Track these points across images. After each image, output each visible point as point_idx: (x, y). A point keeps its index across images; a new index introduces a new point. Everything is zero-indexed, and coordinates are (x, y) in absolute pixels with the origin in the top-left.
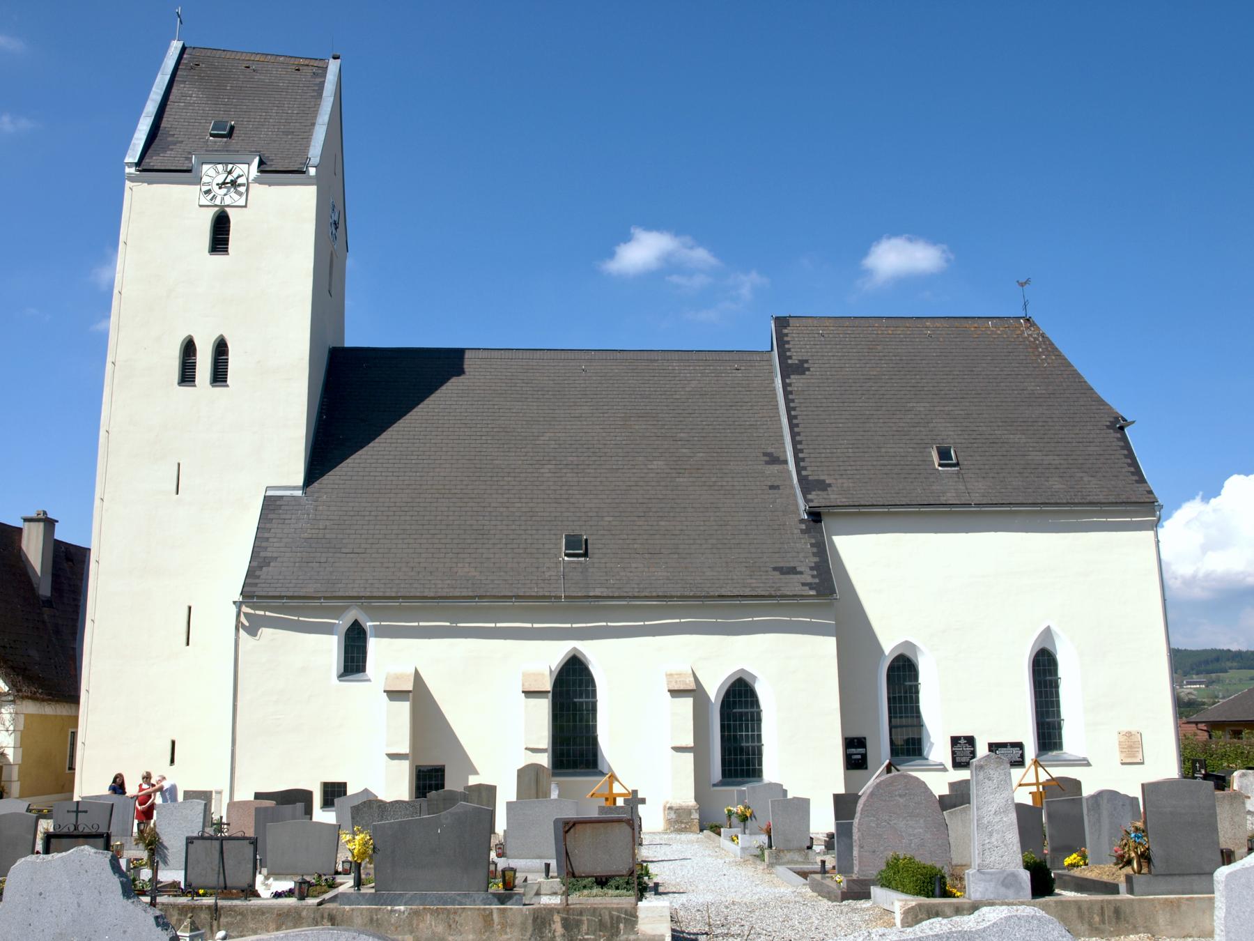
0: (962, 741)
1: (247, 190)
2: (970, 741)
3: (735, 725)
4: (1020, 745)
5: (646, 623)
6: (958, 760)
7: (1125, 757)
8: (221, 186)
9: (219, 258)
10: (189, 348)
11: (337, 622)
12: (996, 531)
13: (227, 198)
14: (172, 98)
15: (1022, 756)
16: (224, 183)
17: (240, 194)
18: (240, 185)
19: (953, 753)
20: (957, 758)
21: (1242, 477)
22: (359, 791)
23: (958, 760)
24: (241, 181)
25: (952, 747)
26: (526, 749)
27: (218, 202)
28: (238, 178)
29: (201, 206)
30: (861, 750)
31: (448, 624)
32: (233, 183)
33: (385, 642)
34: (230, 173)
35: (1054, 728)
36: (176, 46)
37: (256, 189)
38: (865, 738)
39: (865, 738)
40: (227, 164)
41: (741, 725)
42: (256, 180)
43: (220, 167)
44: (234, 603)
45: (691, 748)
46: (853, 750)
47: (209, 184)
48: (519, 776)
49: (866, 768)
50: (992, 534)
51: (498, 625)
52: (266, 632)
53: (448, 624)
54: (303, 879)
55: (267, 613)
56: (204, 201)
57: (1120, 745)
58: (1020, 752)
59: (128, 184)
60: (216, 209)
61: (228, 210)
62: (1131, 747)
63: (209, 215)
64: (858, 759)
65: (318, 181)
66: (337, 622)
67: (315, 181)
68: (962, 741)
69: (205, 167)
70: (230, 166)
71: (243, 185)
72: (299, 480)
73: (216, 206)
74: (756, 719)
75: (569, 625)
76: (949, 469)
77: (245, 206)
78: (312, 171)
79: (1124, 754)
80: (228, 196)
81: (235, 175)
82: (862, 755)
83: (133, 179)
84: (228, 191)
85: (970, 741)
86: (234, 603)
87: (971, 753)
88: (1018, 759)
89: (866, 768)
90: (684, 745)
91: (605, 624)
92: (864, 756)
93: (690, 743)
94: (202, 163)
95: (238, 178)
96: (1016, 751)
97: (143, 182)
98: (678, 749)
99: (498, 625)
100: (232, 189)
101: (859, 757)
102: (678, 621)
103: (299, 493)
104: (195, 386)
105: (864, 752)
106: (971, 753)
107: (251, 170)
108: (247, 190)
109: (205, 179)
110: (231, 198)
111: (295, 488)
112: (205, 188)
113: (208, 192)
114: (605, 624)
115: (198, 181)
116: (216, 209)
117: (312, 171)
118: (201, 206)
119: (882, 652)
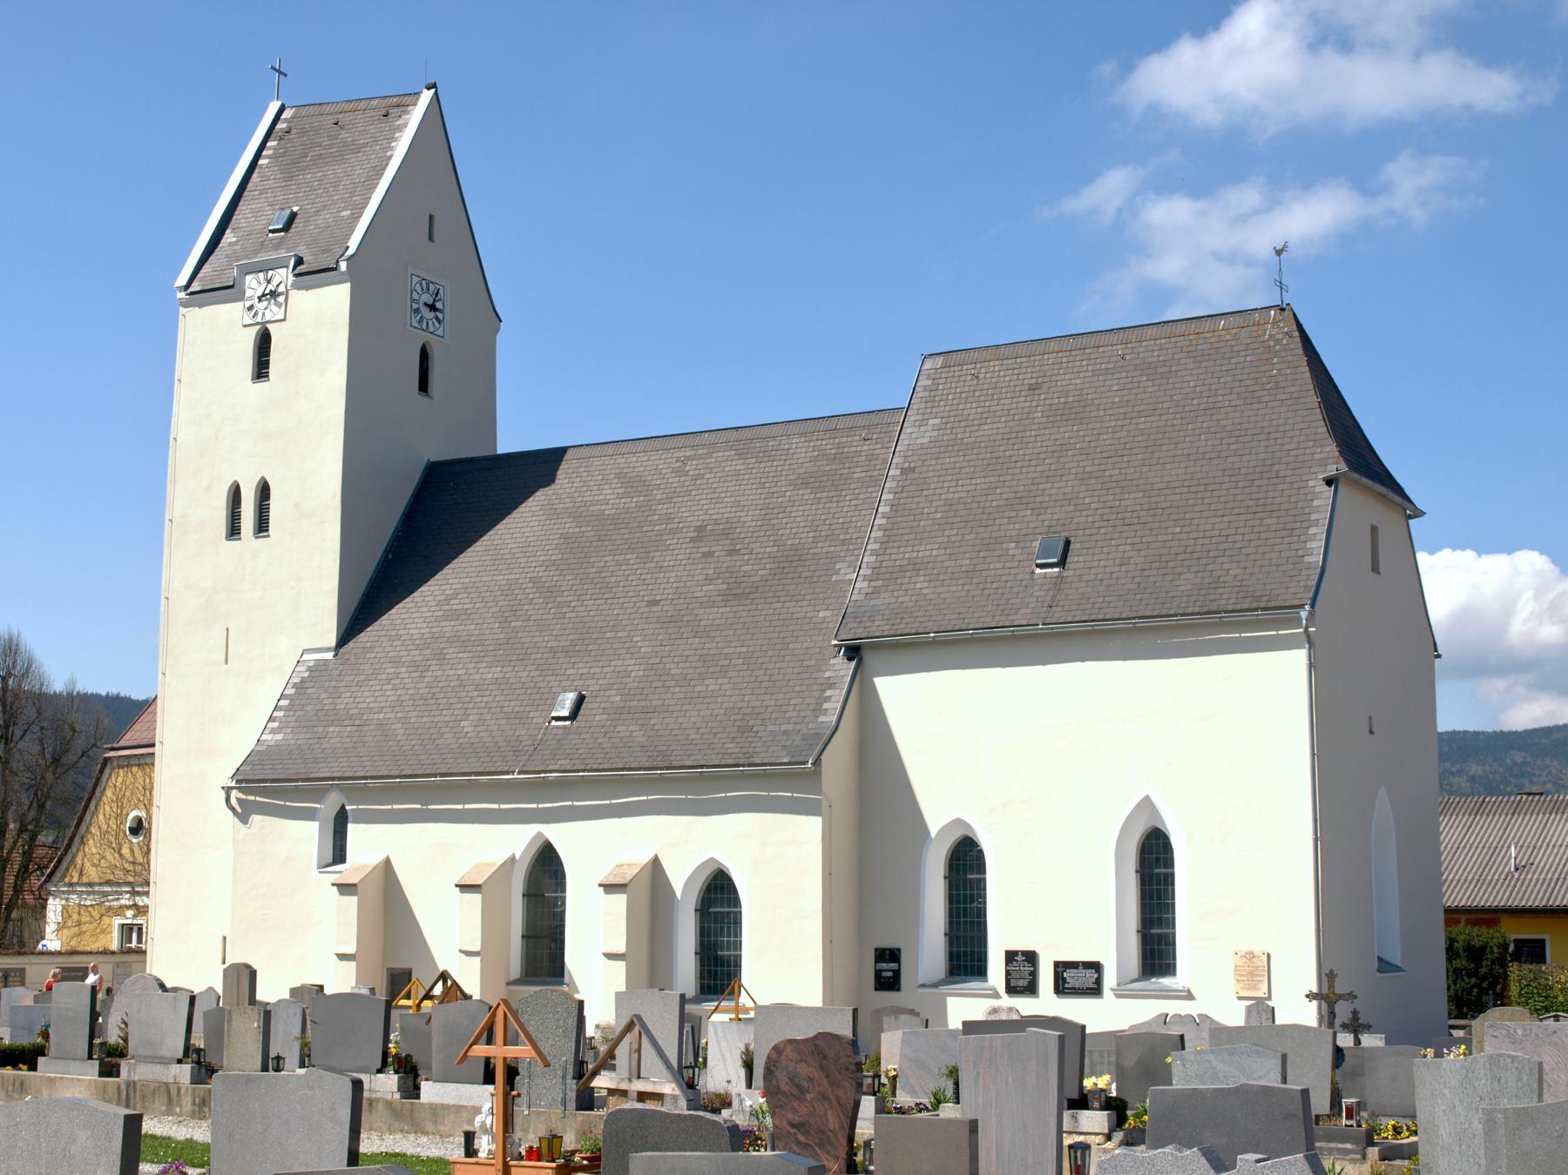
0: (1020, 958)
1: (286, 300)
2: (1031, 957)
3: (716, 928)
4: (1096, 967)
5: (613, 801)
6: (1013, 983)
7: (1242, 988)
8: (260, 299)
9: (262, 386)
10: (235, 495)
11: (318, 806)
12: (1083, 660)
13: (267, 312)
14: (250, 186)
15: (1099, 981)
16: (264, 295)
17: (279, 305)
18: (279, 295)
19: (1008, 973)
20: (1012, 981)
21: (1469, 554)
22: (803, 1004)
23: (1013, 983)
24: (282, 289)
25: (1007, 965)
26: (460, 951)
27: (259, 319)
28: (278, 286)
29: (245, 326)
30: (894, 966)
31: (419, 806)
32: (274, 294)
33: (362, 826)
34: (269, 282)
35: (1167, 944)
36: (274, 107)
37: (295, 295)
38: (899, 950)
39: (899, 950)
40: (267, 270)
41: (722, 929)
42: (296, 286)
43: (261, 275)
44: (223, 788)
45: (623, 955)
46: (884, 966)
47: (251, 298)
48: (224, 975)
49: (899, 990)
50: (1078, 665)
51: (467, 806)
52: (256, 819)
53: (419, 806)
54: (858, 1148)
55: (258, 799)
56: (248, 321)
57: (1236, 970)
58: (1096, 976)
59: (182, 310)
60: (259, 327)
61: (268, 326)
62: (1252, 974)
63: (251, 335)
64: (890, 978)
65: (353, 276)
66: (318, 806)
67: (347, 277)
68: (1020, 958)
69: (249, 278)
70: (270, 273)
71: (282, 294)
72: (331, 640)
73: (258, 323)
74: (736, 921)
75: (608, 802)
76: (1049, 570)
77: (284, 320)
78: (343, 266)
79: (1241, 985)
80: (268, 310)
81: (275, 282)
82: (893, 971)
83: (186, 304)
84: (269, 303)
85: (1031, 957)
86: (223, 788)
87: (1030, 975)
88: (1092, 986)
89: (899, 990)
90: (615, 951)
91: (570, 803)
92: (897, 974)
93: (476, 947)
94: (246, 274)
95: (278, 286)
96: (1091, 975)
97: (195, 306)
98: (611, 956)
99: (467, 806)
100: (273, 301)
101: (890, 974)
102: (645, 798)
103: (330, 655)
104: (240, 539)
105: (896, 968)
106: (1030, 975)
107: (283, 276)
108: (286, 300)
109: (249, 293)
110: (272, 312)
111: (327, 650)
112: (248, 304)
113: (251, 308)
114: (570, 803)
115: (241, 297)
116: (259, 327)
117: (343, 266)
118: (245, 326)
119: (928, 832)
